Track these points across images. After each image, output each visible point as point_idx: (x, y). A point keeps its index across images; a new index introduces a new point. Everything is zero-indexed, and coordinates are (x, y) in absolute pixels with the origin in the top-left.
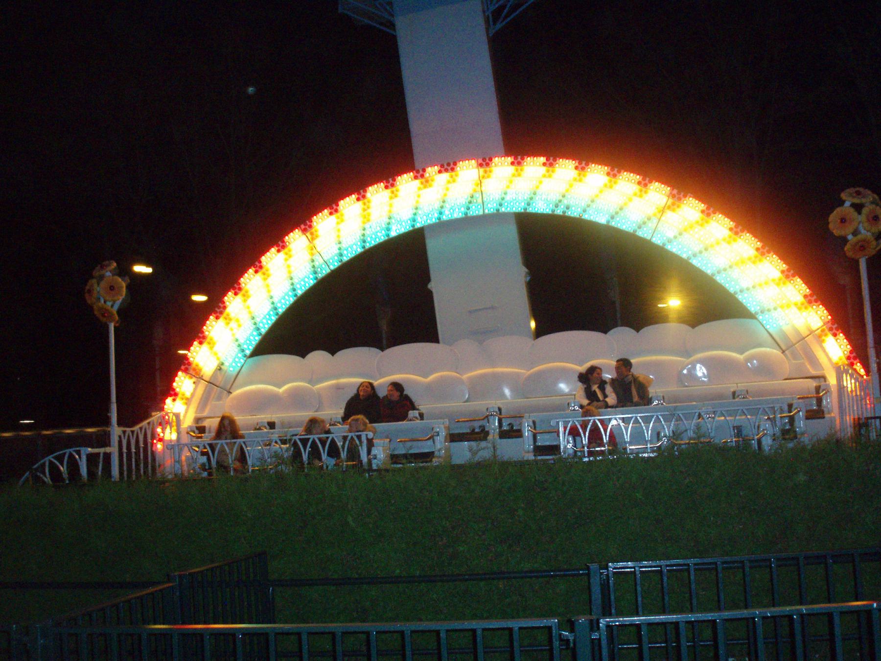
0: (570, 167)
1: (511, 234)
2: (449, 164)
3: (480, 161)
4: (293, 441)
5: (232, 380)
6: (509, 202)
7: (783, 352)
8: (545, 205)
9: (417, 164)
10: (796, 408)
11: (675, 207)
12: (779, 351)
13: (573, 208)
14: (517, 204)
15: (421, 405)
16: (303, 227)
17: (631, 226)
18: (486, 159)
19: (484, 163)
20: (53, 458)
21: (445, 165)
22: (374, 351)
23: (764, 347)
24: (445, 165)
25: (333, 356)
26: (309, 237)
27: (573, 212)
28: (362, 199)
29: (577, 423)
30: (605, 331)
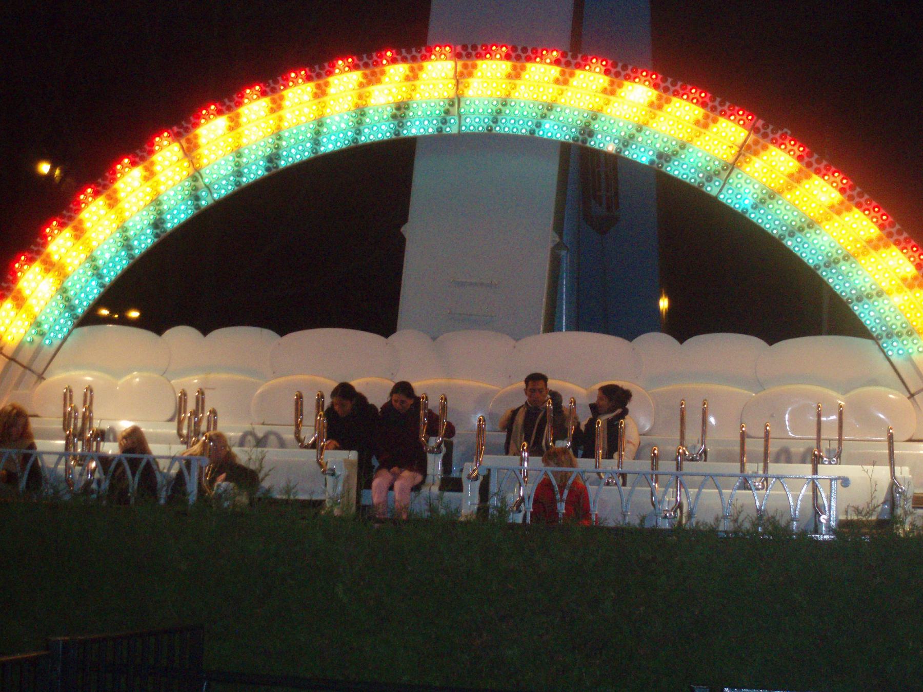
0: (598, 70)
1: (550, 169)
2: (525, 50)
3: (459, 49)
4: (143, 463)
5: (49, 358)
6: (517, 119)
7: (912, 396)
8: (556, 127)
9: (428, 44)
10: (206, 467)
11: (759, 147)
12: (903, 393)
13: (599, 136)
14: (512, 122)
15: (45, 417)
16: (176, 129)
17: (687, 172)
18: (477, 47)
19: (464, 53)
20: (552, 472)
21: (519, 48)
22: (267, 335)
23: (881, 386)
24: (519, 48)
25: (681, 343)
26: (185, 145)
27: (597, 142)
28: (270, 93)
29: (551, 476)
30: (282, 332)
